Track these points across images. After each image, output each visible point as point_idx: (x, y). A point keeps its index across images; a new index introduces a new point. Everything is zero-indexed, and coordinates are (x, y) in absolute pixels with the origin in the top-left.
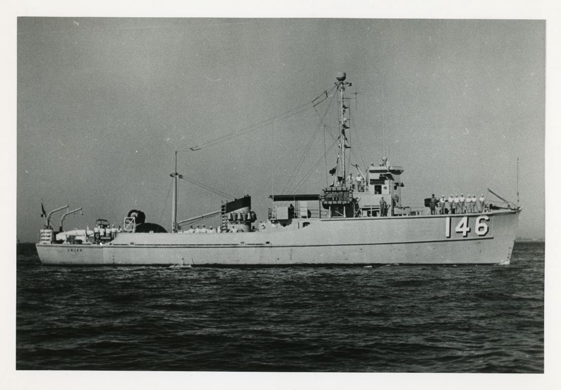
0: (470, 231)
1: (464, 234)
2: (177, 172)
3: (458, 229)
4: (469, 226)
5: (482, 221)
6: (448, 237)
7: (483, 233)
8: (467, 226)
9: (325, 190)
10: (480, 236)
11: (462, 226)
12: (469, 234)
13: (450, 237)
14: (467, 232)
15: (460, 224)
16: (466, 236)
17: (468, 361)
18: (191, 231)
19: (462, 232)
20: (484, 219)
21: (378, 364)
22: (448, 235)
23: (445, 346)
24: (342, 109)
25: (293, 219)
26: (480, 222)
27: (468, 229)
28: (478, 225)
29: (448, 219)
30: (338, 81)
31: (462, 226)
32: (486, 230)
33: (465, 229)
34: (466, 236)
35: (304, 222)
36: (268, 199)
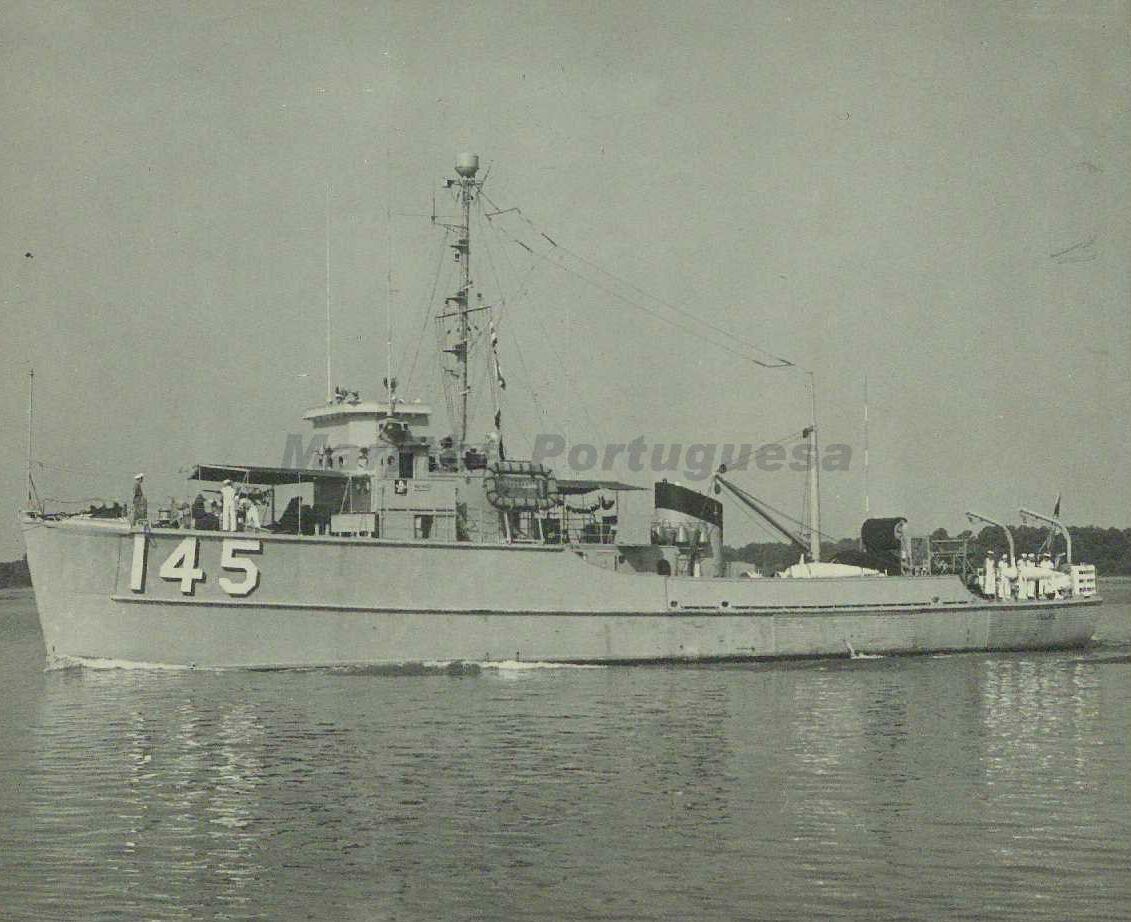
0: (203, 580)
1: (186, 587)
3: (168, 570)
6: (136, 592)
7: (243, 588)
9: (495, 469)
11: (179, 564)
12: (199, 587)
13: (142, 591)
15: (175, 558)
16: (192, 593)
18: (399, 409)
24: (486, 220)
29: (140, 542)
30: (459, 176)
31: (179, 564)
32: (251, 582)
33: (188, 573)
34: (192, 593)
36: (186, 482)
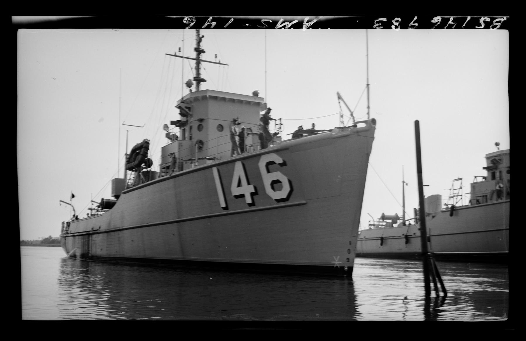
2: (182, 42)
4: (250, 180)
5: (270, 167)
7: (283, 194)
8: (249, 184)
10: (279, 201)
11: (239, 185)
14: (252, 195)
16: (252, 204)
17: (476, 292)
19: (243, 196)
20: (272, 163)
21: (460, 272)
22: (223, 205)
23: (498, 280)
25: (353, 124)
26: (269, 171)
27: (251, 189)
28: (267, 179)
31: (239, 185)
32: (286, 189)
33: (247, 190)
35: (267, 148)
